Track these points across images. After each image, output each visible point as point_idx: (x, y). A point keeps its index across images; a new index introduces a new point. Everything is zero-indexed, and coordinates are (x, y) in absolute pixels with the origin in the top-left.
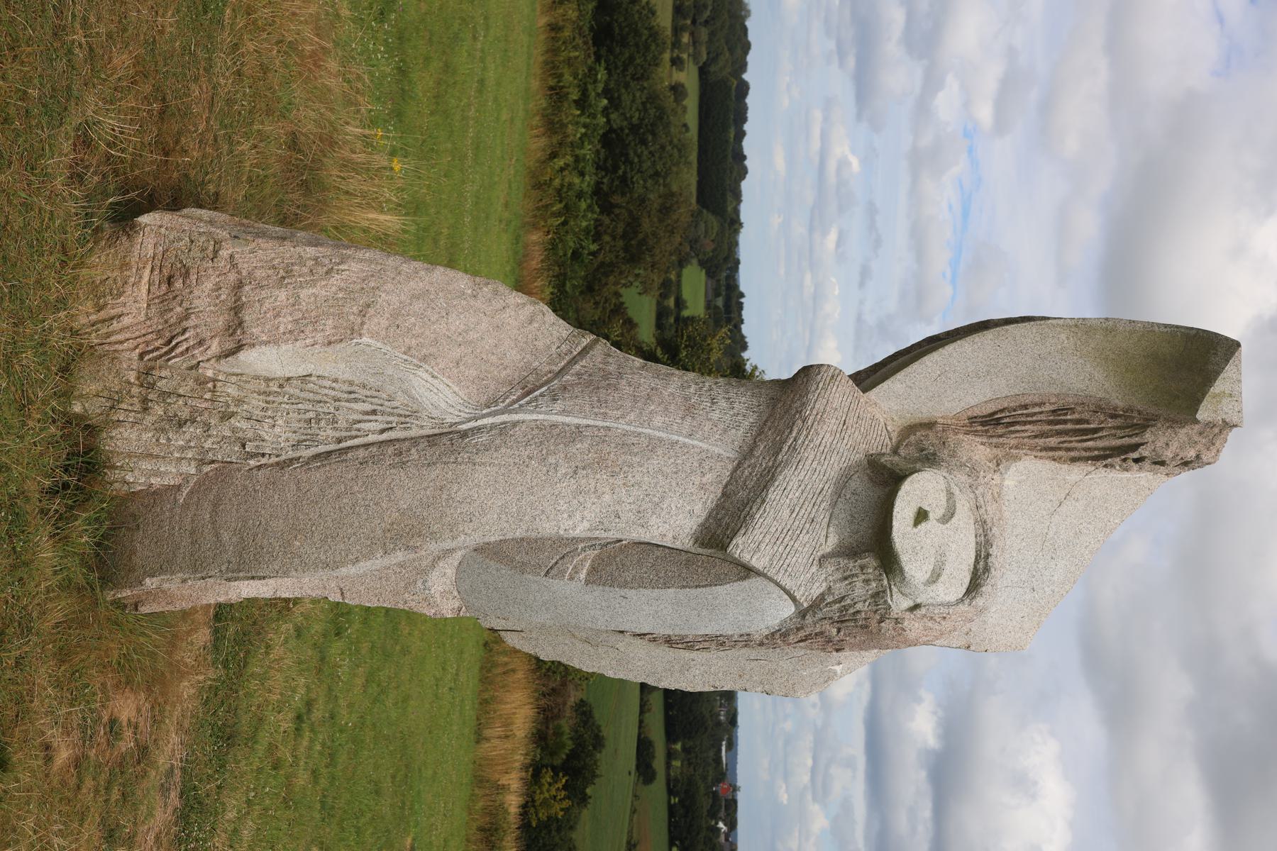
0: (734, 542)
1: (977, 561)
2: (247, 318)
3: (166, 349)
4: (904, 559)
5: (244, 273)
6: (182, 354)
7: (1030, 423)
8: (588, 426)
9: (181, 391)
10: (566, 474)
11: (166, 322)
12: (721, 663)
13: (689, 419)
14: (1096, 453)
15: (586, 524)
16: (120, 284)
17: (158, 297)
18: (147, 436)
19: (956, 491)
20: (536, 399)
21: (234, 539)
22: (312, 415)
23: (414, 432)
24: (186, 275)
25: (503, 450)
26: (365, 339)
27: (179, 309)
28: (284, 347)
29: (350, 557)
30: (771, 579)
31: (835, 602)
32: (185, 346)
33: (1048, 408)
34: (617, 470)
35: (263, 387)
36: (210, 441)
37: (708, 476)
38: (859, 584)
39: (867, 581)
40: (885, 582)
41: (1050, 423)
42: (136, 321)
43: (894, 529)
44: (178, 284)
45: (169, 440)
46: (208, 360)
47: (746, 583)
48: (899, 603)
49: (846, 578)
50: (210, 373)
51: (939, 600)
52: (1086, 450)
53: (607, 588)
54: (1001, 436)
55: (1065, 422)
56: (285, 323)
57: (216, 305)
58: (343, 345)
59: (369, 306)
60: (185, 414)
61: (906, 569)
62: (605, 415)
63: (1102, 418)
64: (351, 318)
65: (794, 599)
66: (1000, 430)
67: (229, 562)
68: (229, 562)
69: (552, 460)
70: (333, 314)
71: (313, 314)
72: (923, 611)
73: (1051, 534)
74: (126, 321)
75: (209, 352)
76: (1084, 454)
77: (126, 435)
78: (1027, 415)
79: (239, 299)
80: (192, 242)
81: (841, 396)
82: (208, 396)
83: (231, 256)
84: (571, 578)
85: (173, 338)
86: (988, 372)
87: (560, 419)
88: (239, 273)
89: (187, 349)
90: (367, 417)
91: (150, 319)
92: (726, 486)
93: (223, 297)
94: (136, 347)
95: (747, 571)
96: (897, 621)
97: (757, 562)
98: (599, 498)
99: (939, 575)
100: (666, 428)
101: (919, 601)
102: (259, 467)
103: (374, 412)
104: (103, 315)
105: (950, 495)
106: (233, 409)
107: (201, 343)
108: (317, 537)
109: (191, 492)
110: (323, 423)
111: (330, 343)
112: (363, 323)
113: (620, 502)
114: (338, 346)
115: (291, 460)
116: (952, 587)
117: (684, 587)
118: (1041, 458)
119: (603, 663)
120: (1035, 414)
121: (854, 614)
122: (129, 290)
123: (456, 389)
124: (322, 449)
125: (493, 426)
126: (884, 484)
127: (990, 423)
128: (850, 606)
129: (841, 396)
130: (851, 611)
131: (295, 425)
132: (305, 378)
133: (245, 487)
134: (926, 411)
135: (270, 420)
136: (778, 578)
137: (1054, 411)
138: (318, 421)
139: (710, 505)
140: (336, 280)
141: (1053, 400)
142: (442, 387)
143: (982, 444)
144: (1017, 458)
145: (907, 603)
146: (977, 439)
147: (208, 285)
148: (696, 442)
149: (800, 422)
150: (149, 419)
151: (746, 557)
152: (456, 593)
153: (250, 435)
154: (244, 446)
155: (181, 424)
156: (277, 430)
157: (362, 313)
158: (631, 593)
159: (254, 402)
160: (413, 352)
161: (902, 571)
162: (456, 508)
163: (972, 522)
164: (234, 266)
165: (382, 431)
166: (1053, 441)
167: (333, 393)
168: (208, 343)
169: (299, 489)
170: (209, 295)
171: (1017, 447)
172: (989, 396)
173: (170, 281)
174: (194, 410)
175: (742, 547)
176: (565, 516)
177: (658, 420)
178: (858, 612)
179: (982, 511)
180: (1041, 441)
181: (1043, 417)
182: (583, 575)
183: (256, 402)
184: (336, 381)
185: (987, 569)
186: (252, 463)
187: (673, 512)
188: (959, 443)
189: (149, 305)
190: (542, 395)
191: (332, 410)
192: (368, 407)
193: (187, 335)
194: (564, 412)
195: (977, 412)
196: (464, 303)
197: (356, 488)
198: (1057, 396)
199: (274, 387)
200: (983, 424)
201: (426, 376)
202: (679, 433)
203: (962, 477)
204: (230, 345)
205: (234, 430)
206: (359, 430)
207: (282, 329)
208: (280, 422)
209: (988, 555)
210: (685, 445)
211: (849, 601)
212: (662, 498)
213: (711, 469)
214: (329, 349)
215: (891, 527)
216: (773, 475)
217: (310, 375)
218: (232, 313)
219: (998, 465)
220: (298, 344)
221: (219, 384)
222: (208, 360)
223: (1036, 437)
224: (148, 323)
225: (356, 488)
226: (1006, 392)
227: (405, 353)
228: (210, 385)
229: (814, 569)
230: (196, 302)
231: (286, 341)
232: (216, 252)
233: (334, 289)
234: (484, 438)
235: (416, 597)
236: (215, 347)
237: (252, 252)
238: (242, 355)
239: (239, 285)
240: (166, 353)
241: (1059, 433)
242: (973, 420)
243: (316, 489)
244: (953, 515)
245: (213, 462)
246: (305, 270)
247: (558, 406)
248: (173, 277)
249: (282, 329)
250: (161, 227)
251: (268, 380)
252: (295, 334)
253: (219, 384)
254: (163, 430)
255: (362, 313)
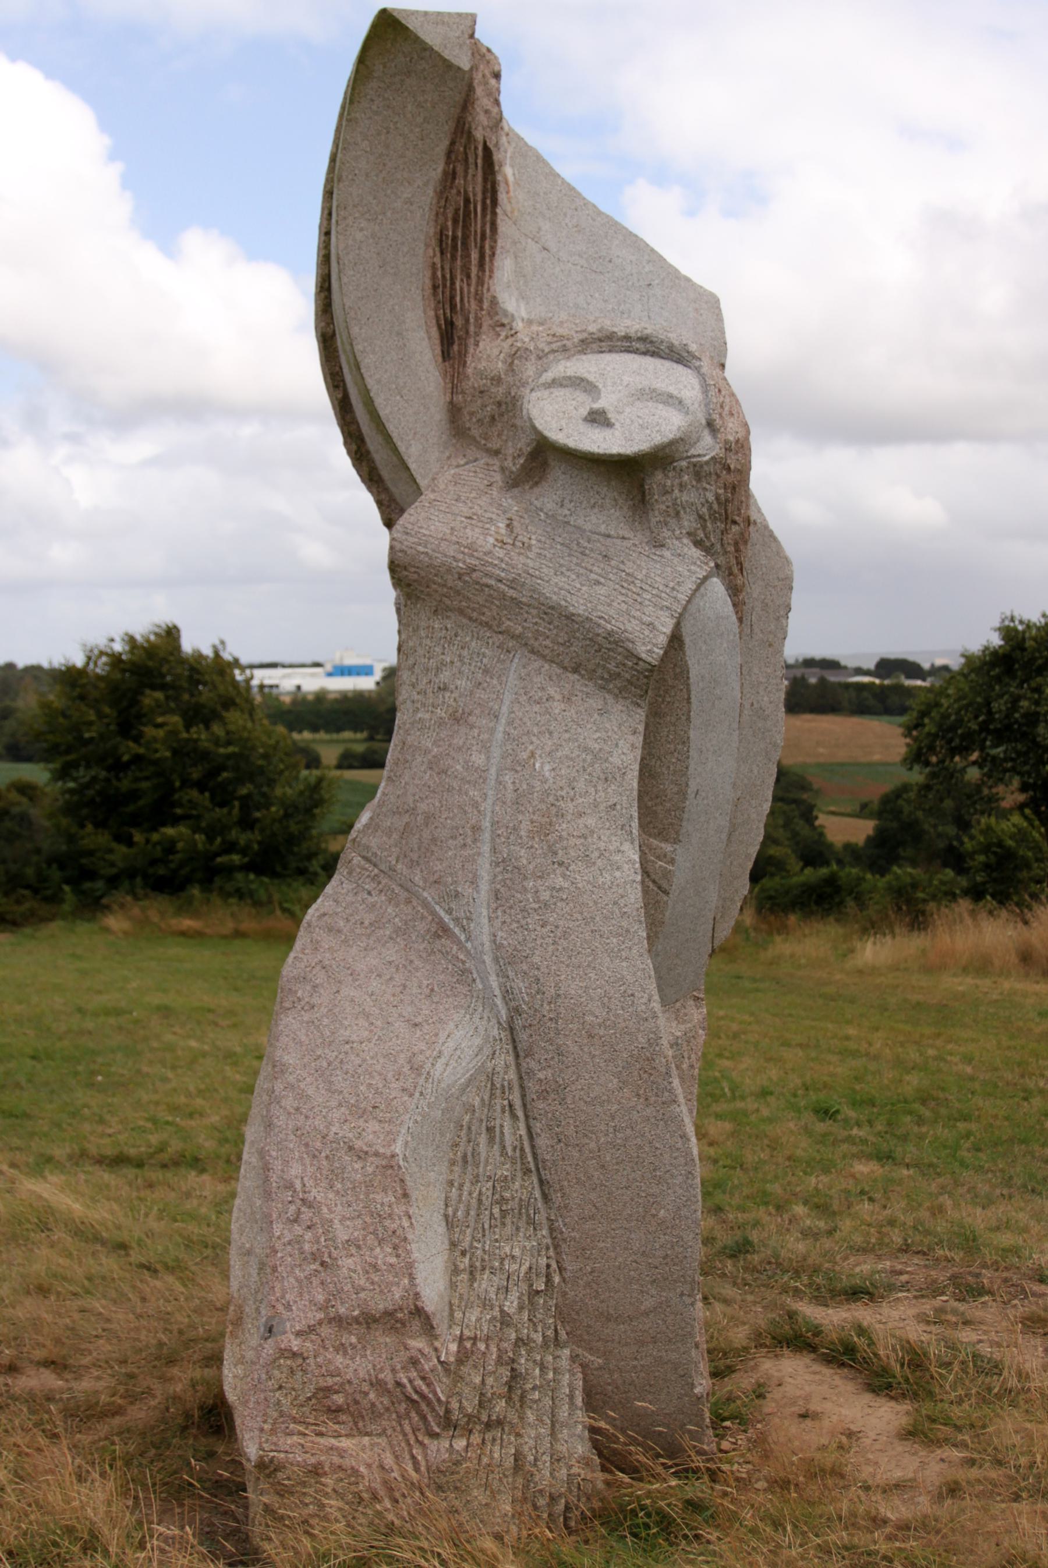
0: (643, 656)
1: (636, 351)
2: (381, 1307)
3: (423, 1406)
4: (658, 439)
5: (320, 1315)
6: (429, 1385)
7: (453, 283)
8: (494, 850)
9: (478, 1380)
10: (564, 876)
11: (387, 1409)
12: (756, 670)
13: (472, 719)
14: (488, 201)
15: (626, 846)
16: (341, 1475)
17: (356, 1423)
18: (531, 1416)
19: (548, 376)
20: (456, 920)
21: (653, 1292)
22: (496, 1211)
23: (512, 1075)
24: (328, 1390)
25: (536, 959)
26: (398, 1148)
27: (372, 1396)
28: (416, 1255)
29: (679, 1145)
30: (685, 608)
31: (704, 528)
32: (419, 1382)
33: (437, 260)
34: (554, 810)
35: (465, 1276)
36: (534, 1336)
37: (552, 693)
38: (685, 497)
39: (682, 487)
40: (684, 463)
41: (454, 258)
42: (388, 1447)
43: (622, 451)
44: (339, 1399)
45: (534, 1388)
46: (436, 1350)
47: (687, 640)
48: (707, 447)
49: (678, 513)
50: (454, 1347)
51: (700, 396)
52: (484, 215)
53: (686, 816)
54: (467, 320)
55: (455, 238)
56: (383, 1255)
57: (364, 1347)
58: (407, 1178)
59: (351, 1148)
60: (505, 1373)
61: (671, 436)
62: (476, 829)
63: (454, 191)
64: (370, 1170)
65: (705, 579)
66: (459, 322)
67: (682, 1294)
68: (682, 1294)
69: (545, 895)
70: (367, 1195)
71: (368, 1219)
72: (716, 416)
73: (583, 262)
74: (389, 1460)
75: (426, 1350)
76: (488, 217)
77: (532, 1443)
78: (444, 286)
79: (356, 1320)
80: (280, 1388)
81: (431, 522)
82: (482, 1346)
83: (298, 1334)
84: (672, 861)
85: (409, 1399)
86: (399, 334)
87: (484, 887)
88: (320, 1323)
89: (423, 1378)
90: (497, 1139)
91: (384, 1430)
92: (565, 668)
93: (354, 1339)
94: (421, 1443)
95: (676, 640)
96: (728, 449)
97: (666, 626)
98: (592, 832)
99: (671, 396)
100: (486, 748)
101: (704, 422)
102: (561, 1269)
103: (490, 1130)
104: (382, 1493)
105: (555, 383)
106: (496, 1313)
107: (414, 1362)
108: (655, 1190)
109: (590, 1350)
110: (507, 1195)
111: (405, 1195)
112: (376, 1154)
113: (596, 805)
114: (409, 1183)
115: (551, 1230)
116: (684, 383)
117: (688, 719)
118: (491, 271)
119: (754, 816)
120: (444, 276)
121: (719, 503)
122: (348, 1462)
123: (452, 1025)
124: (537, 1194)
125: (502, 974)
126: (544, 466)
127: (452, 339)
128: (710, 508)
129: (431, 522)
130: (715, 506)
131: (509, 1229)
132: (450, 1223)
133: (588, 1285)
134: (437, 413)
135: (506, 1262)
136: (683, 598)
137: (442, 253)
138: (503, 1200)
139: (590, 688)
140: (316, 1193)
141: (431, 252)
142: (451, 1044)
143: (477, 345)
144: (494, 302)
145: (707, 439)
146: (471, 350)
147: (339, 1360)
148: (505, 709)
149: (474, 575)
150: (513, 1416)
151: (662, 640)
152: (678, 1004)
153: (524, 1287)
154: (538, 1292)
155: (515, 1375)
156: (517, 1252)
157: (362, 1156)
158: (693, 786)
159: (484, 1286)
160: (409, 1085)
161: (672, 443)
162: (617, 1016)
163: (584, 357)
164: (311, 1329)
165: (514, 1116)
166: (474, 255)
167: (467, 1185)
168: (414, 1353)
169: (592, 1217)
170: (352, 1359)
171: (481, 301)
172: (422, 334)
173: (335, 1411)
174: (499, 1361)
175: (651, 646)
176: (618, 874)
177: (478, 759)
178: (717, 498)
179: (569, 344)
180: (474, 271)
181: (447, 267)
182: (668, 847)
183: (486, 1284)
184: (451, 1183)
185: (643, 339)
186: (557, 1279)
187: (603, 735)
188: (481, 374)
189: (367, 1434)
190: (449, 911)
191: (490, 1184)
192: (483, 1139)
193: (405, 1381)
194: (474, 882)
195: (438, 350)
196: (326, 1021)
197: (593, 1145)
198: (427, 246)
199: (465, 1265)
200: (451, 343)
201: (439, 1066)
202: (492, 731)
203: (529, 370)
204: (416, 1325)
205: (521, 1308)
206: (515, 1149)
207: (393, 1260)
208: (507, 1249)
209: (627, 338)
210: (510, 723)
211: (705, 510)
212: (586, 749)
213: (543, 689)
214: (414, 1195)
215: (620, 455)
216: (552, 608)
217: (446, 1216)
218: (374, 1326)
219: (503, 325)
220: (410, 1237)
221: (467, 1333)
222: (436, 1350)
223: (469, 277)
224: (389, 1432)
225: (593, 1145)
226: (420, 312)
227: (411, 1095)
228: (468, 1344)
229: (667, 554)
230: (362, 1374)
231: (409, 1252)
232: (294, 1355)
233: (331, 1195)
234: (520, 985)
235: (686, 1054)
236: (418, 1344)
237: (288, 1307)
238: (429, 1308)
239: (338, 1321)
240: (429, 1403)
241: (465, 244)
242: (446, 355)
243: (593, 1196)
244: (582, 380)
245: (556, 1330)
246: (308, 1236)
247: (466, 890)
248: (332, 1406)
249: (393, 1260)
250: (262, 1430)
251: (456, 1271)
252: (399, 1243)
253: (467, 1333)
254: (522, 1398)
255: (362, 1156)
